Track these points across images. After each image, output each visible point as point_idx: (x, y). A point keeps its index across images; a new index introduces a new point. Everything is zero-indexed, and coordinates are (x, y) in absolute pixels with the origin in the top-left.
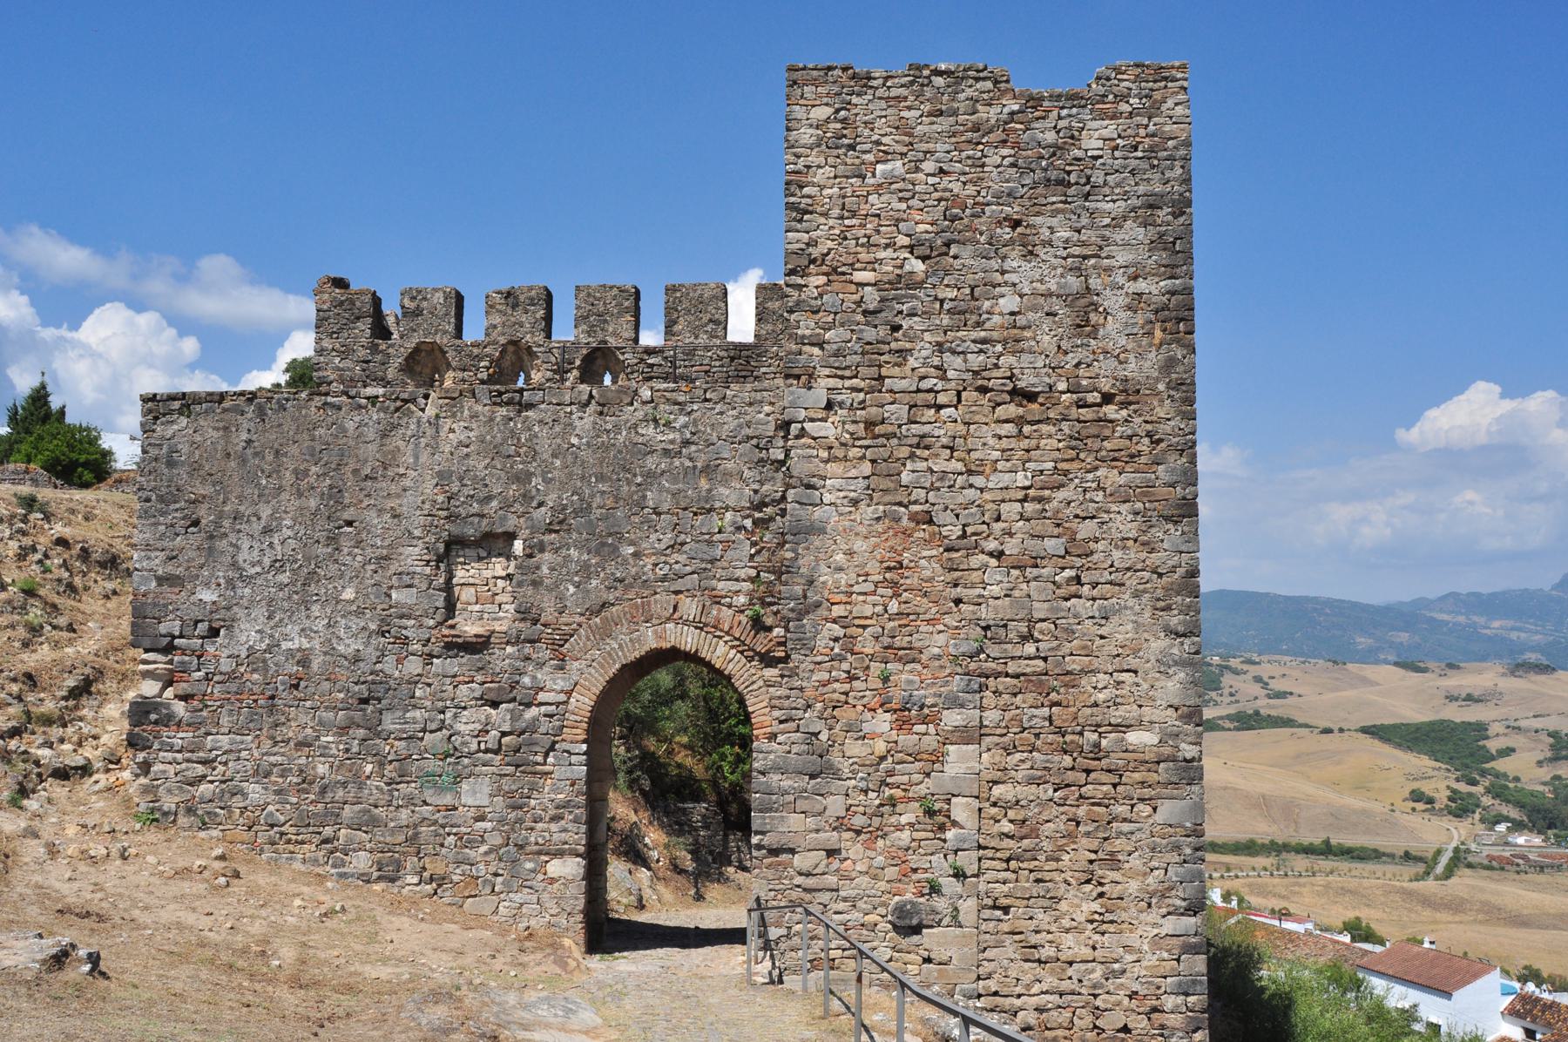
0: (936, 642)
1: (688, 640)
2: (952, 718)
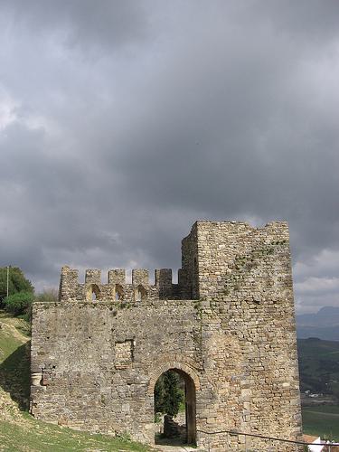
0: (239, 364)
1: (179, 366)
2: (243, 383)
